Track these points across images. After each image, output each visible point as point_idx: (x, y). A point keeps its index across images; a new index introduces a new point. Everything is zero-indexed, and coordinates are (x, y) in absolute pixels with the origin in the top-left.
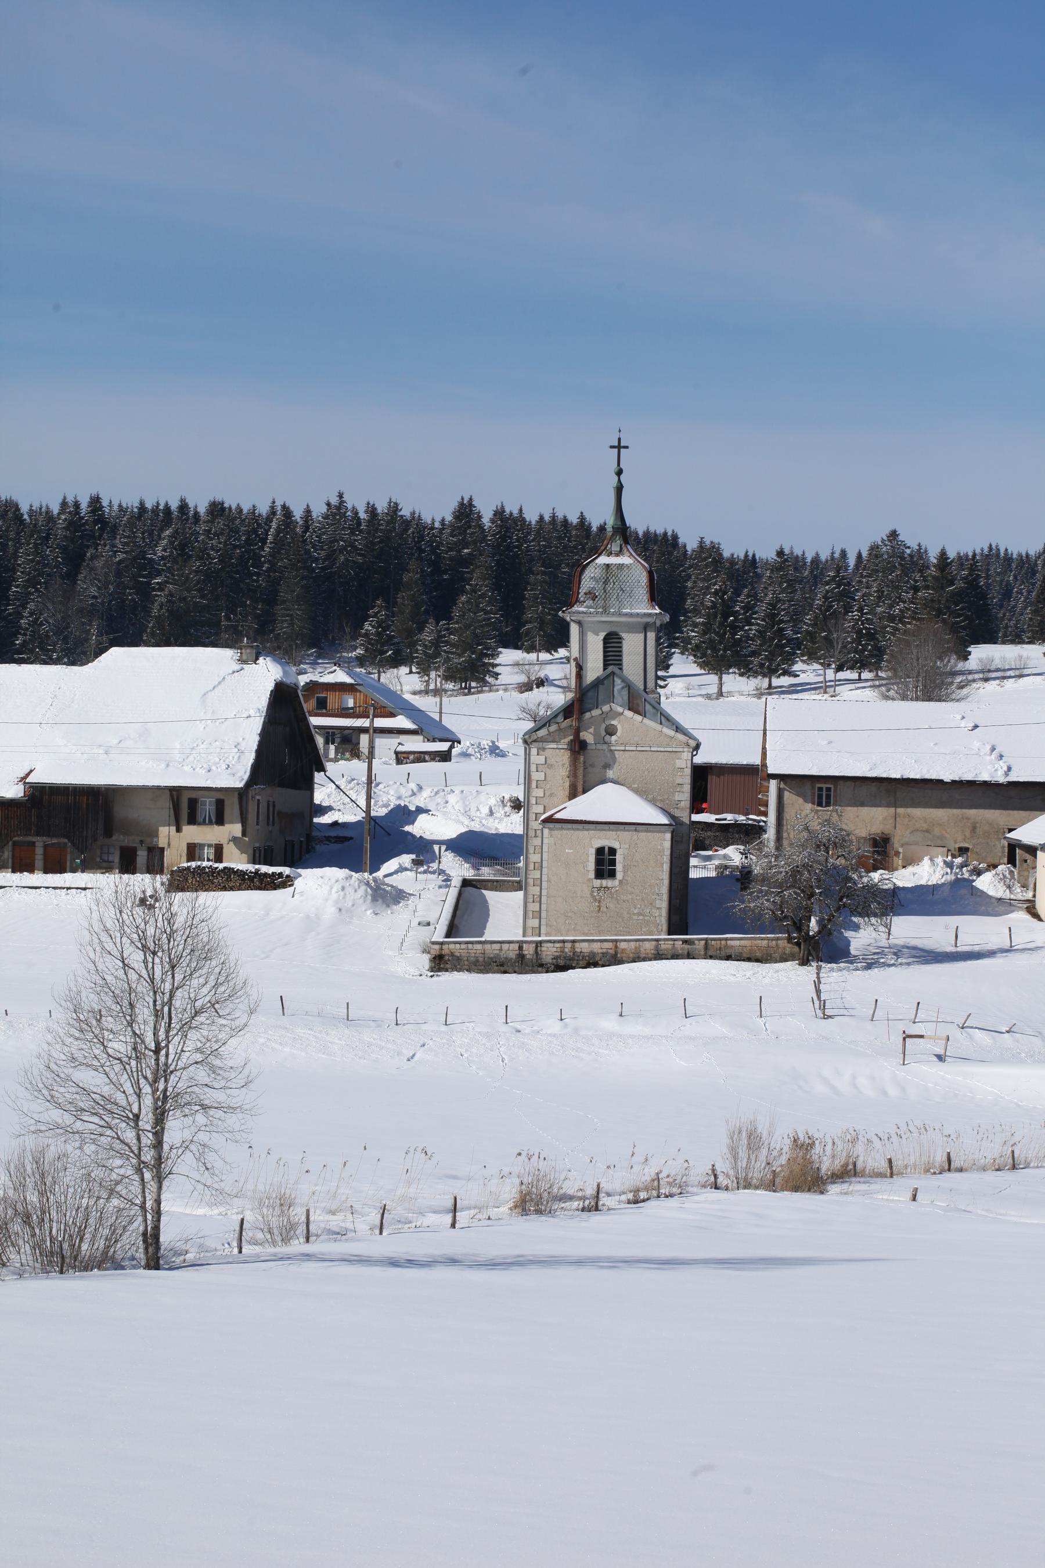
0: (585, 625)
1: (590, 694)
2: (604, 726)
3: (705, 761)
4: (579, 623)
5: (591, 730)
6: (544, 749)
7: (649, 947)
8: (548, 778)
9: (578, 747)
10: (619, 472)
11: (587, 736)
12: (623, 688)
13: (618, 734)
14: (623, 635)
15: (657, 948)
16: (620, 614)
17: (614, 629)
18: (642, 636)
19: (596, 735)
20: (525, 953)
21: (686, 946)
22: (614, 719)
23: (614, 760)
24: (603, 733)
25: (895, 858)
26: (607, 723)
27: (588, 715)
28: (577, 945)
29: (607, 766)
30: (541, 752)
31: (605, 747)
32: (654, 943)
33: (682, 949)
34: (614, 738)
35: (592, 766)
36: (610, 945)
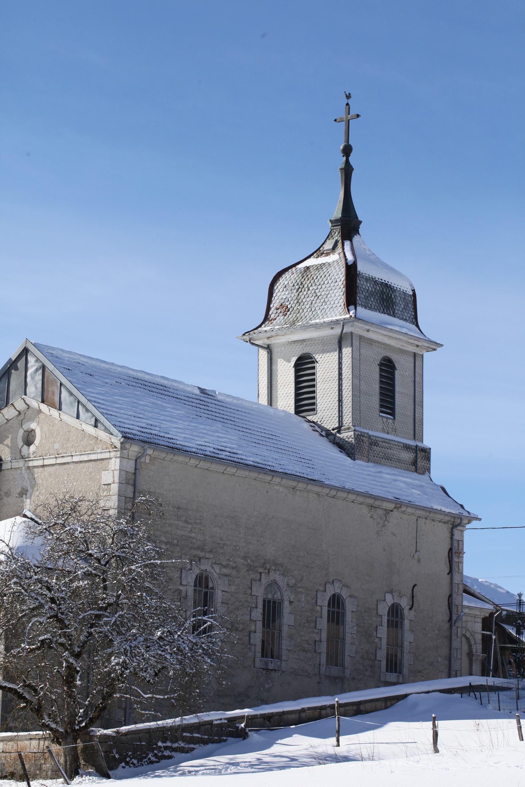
4: (269, 348)
10: (347, 151)
16: (307, 327)
29: (23, 493)
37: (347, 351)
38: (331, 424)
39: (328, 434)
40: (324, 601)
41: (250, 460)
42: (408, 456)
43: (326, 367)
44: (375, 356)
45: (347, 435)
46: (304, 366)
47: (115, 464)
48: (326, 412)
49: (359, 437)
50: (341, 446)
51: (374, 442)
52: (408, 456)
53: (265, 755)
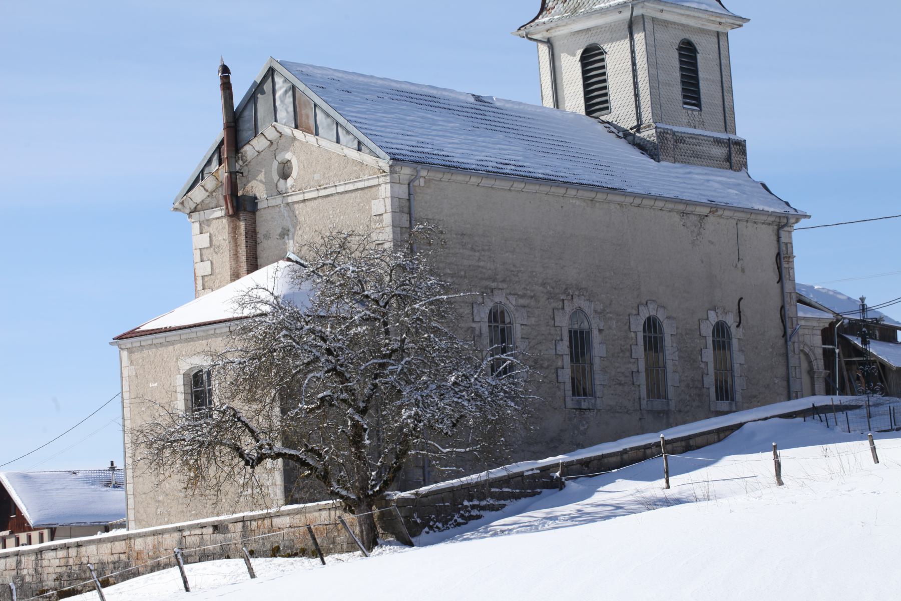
0: (557, 45)
1: (248, 114)
2: (275, 165)
3: (831, 287)
5: (261, 177)
6: (208, 222)
7: (170, 541)
8: (217, 271)
9: (241, 206)
11: (257, 188)
12: (286, 92)
13: (294, 174)
14: (606, 47)
15: (181, 545)
17: (593, 40)
18: (627, 41)
19: (268, 183)
20: (25, 572)
21: (219, 537)
22: (286, 149)
23: (295, 222)
24: (276, 177)
25: (265, 241)
26: (280, 158)
27: (247, 149)
28: (83, 549)
29: (285, 234)
30: (206, 228)
31: (278, 200)
32: (177, 535)
33: (213, 542)
34: (290, 181)
35: (267, 237)
36: (120, 546)
37: (639, 37)
38: (628, 123)
39: (626, 135)
40: (638, 326)
41: (540, 172)
42: (719, 152)
43: (616, 59)
44: (673, 39)
45: (648, 134)
46: (591, 59)
47: (385, 191)
48: (621, 108)
49: (661, 134)
50: (642, 147)
51: (679, 139)
52: (719, 152)
53: (585, 505)
